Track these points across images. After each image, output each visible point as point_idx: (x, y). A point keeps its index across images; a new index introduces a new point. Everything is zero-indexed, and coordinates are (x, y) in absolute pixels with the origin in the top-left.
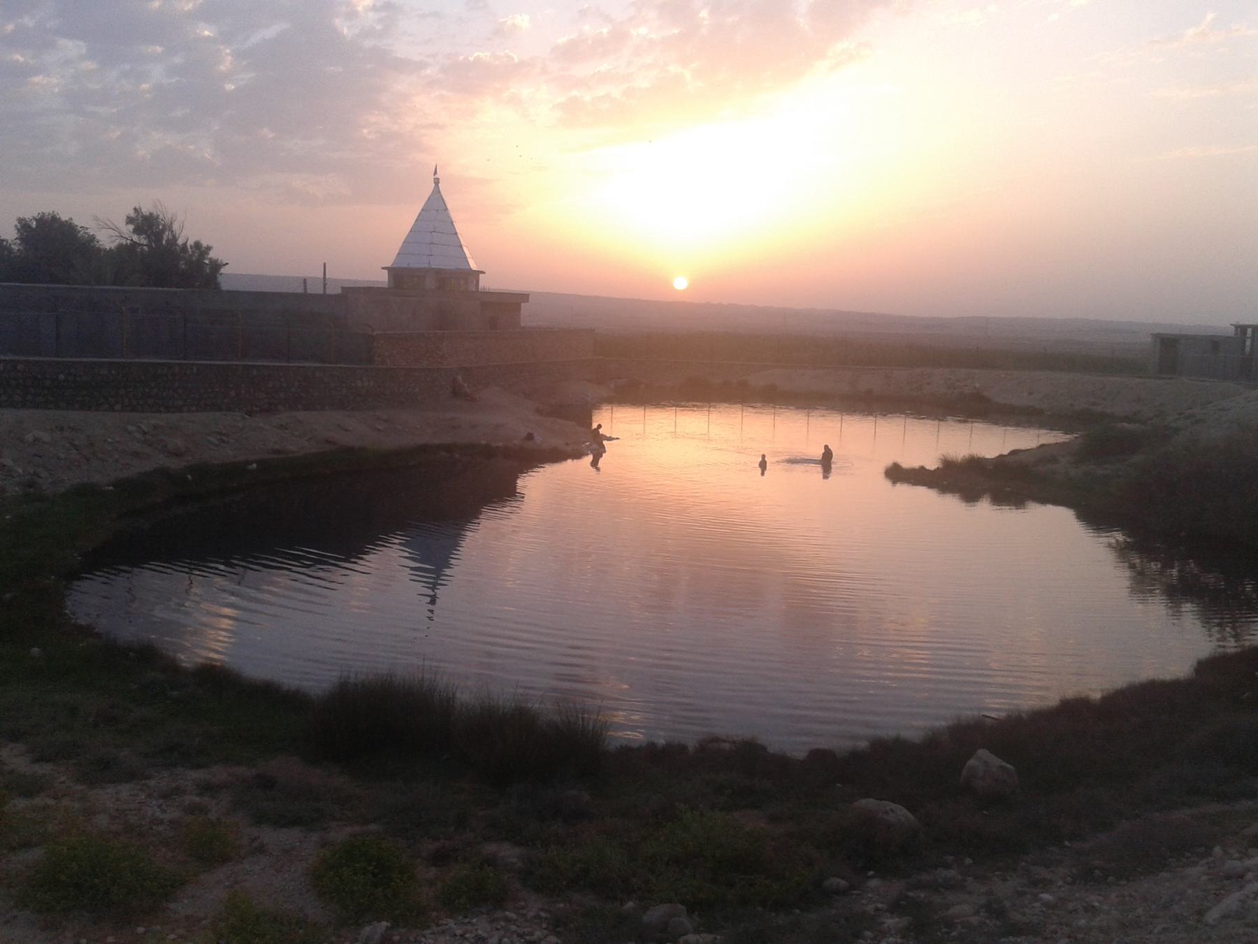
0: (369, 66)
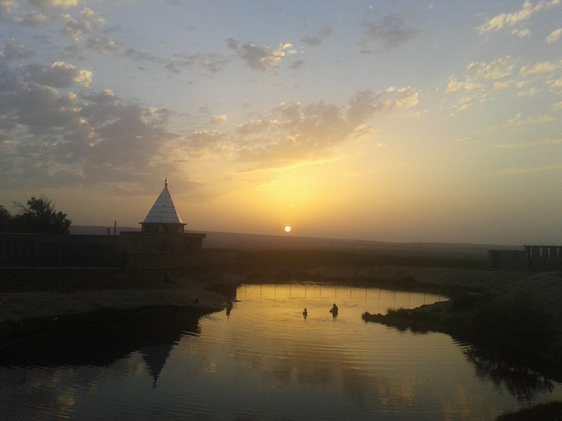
0: (155, 136)
